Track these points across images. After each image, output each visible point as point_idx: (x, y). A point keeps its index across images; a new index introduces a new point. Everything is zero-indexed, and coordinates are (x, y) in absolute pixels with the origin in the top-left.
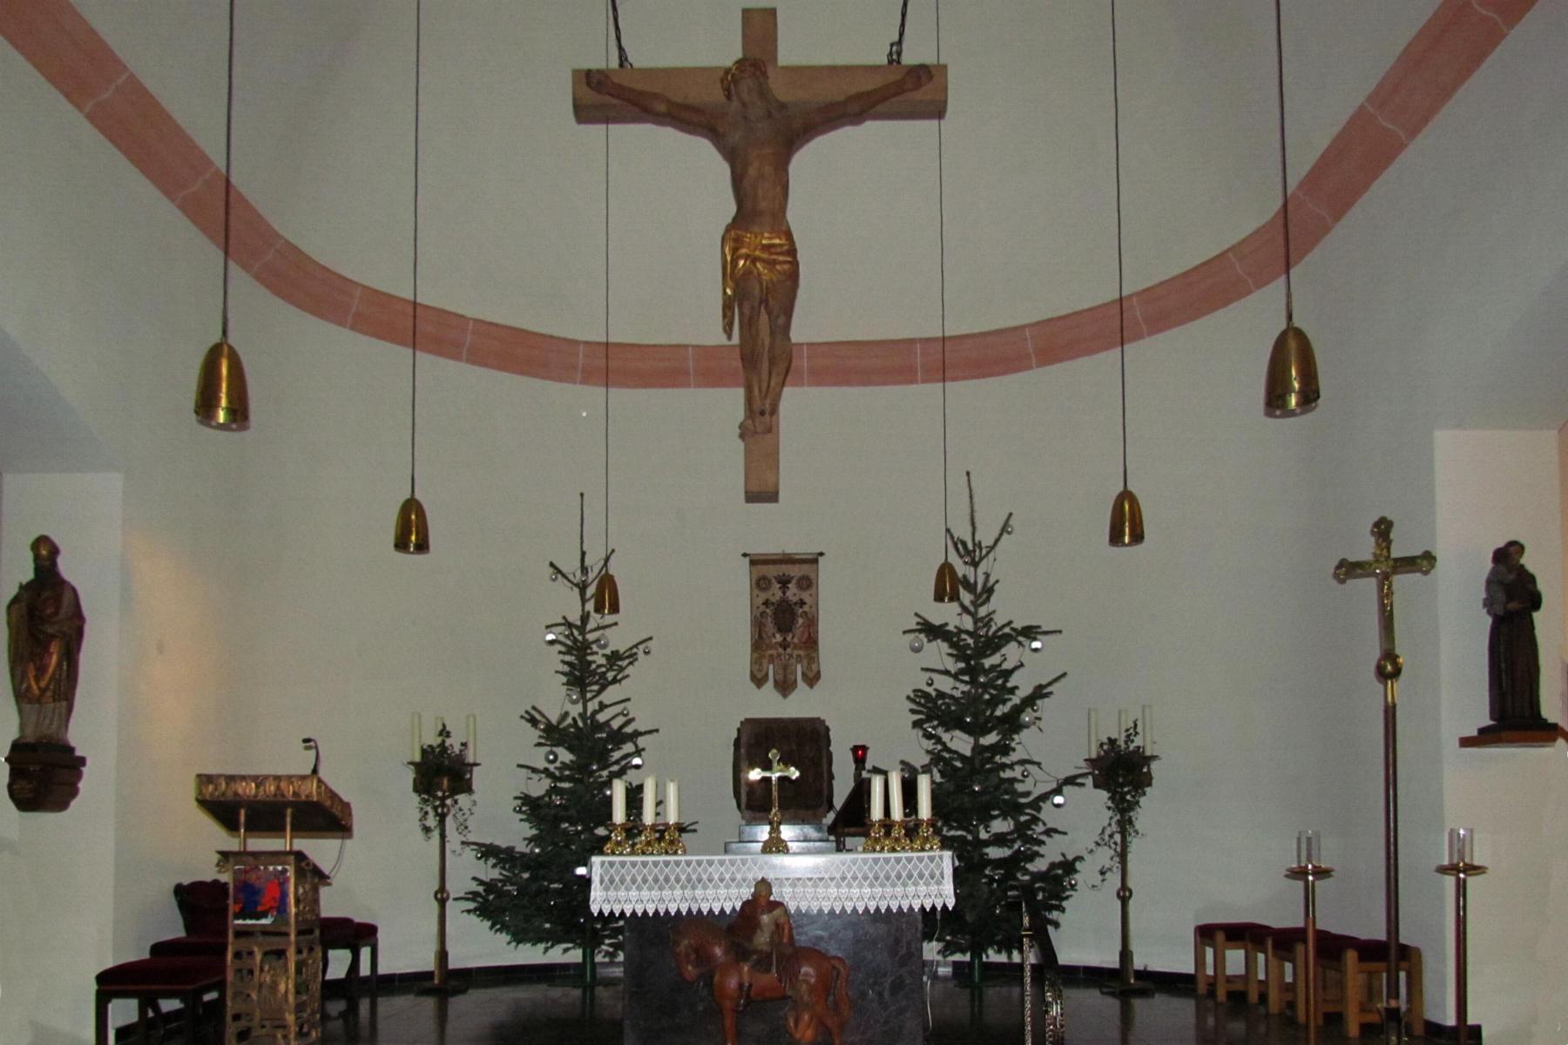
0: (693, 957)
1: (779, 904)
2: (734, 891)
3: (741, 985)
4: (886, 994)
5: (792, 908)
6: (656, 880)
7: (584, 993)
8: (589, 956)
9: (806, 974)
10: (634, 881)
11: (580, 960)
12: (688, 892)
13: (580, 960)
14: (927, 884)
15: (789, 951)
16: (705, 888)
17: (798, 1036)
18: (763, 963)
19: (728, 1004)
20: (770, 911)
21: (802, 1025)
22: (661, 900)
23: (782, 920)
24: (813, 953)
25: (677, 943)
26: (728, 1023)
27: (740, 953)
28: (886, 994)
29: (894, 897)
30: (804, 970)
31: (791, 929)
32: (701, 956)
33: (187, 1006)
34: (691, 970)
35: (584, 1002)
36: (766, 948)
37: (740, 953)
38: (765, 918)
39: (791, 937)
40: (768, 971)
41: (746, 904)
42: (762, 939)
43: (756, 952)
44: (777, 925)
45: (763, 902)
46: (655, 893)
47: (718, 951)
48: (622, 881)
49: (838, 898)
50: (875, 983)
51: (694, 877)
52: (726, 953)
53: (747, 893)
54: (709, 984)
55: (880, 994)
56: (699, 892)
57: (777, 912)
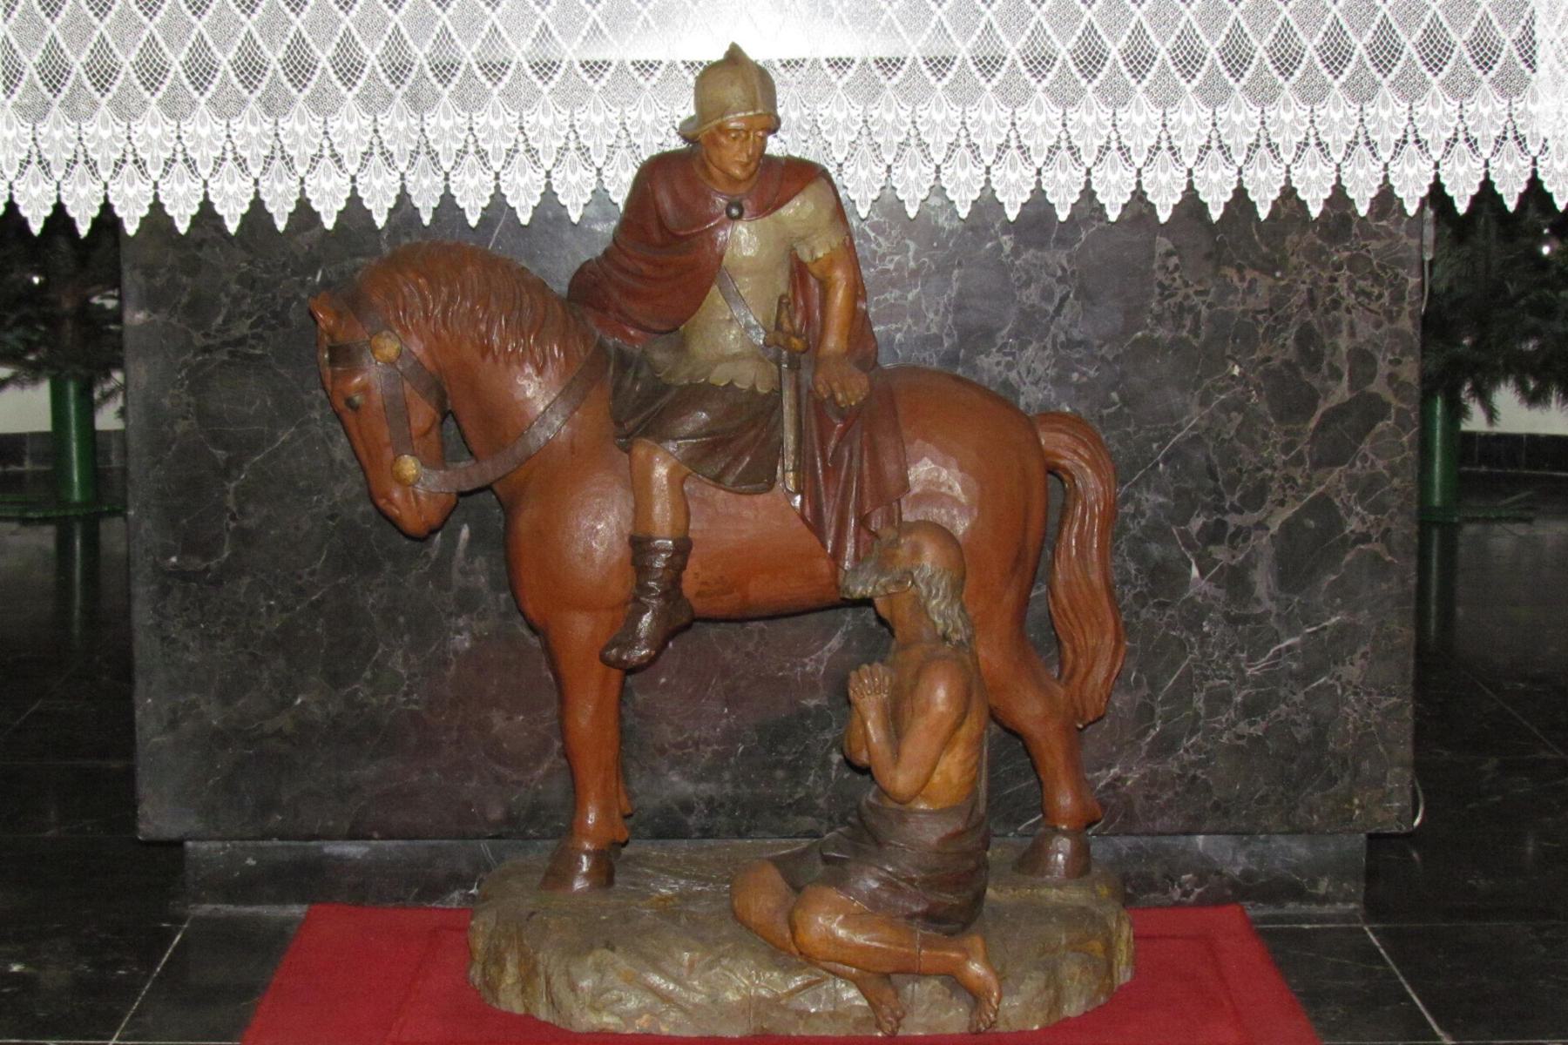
0: (422, 414)
1: (803, 174)
2: (597, 119)
3: (639, 545)
4: (1262, 580)
5: (859, 187)
6: (250, 70)
7: (64, 543)
8: (72, 405)
9: (931, 496)
10: (152, 74)
11: (41, 421)
12: (397, 124)
13: (41, 421)
14: (1460, 90)
15: (852, 390)
16: (468, 101)
17: (902, 780)
18: (738, 441)
19: (582, 629)
20: (768, 206)
21: (919, 743)
22: (277, 157)
23: (820, 249)
24: (944, 394)
25: (345, 357)
26: (585, 715)
27: (635, 404)
28: (1262, 580)
29: (1013, 147)
30: (922, 471)
31: (858, 290)
32: (460, 412)
33: (473, 229)
34: (416, 481)
35: (63, 588)
36: (750, 376)
37: (635, 404)
38: (744, 240)
39: (859, 325)
40: (761, 478)
41: (656, 170)
42: (733, 332)
43: (697, 394)
44: (799, 272)
45: (734, 159)
46: (251, 129)
47: (534, 391)
48: (102, 76)
49: (1013, 147)
50: (1215, 533)
51: (420, 54)
52: (574, 390)
53: (661, 122)
54: (501, 543)
55: (1236, 580)
56: (444, 123)
57: (799, 210)
